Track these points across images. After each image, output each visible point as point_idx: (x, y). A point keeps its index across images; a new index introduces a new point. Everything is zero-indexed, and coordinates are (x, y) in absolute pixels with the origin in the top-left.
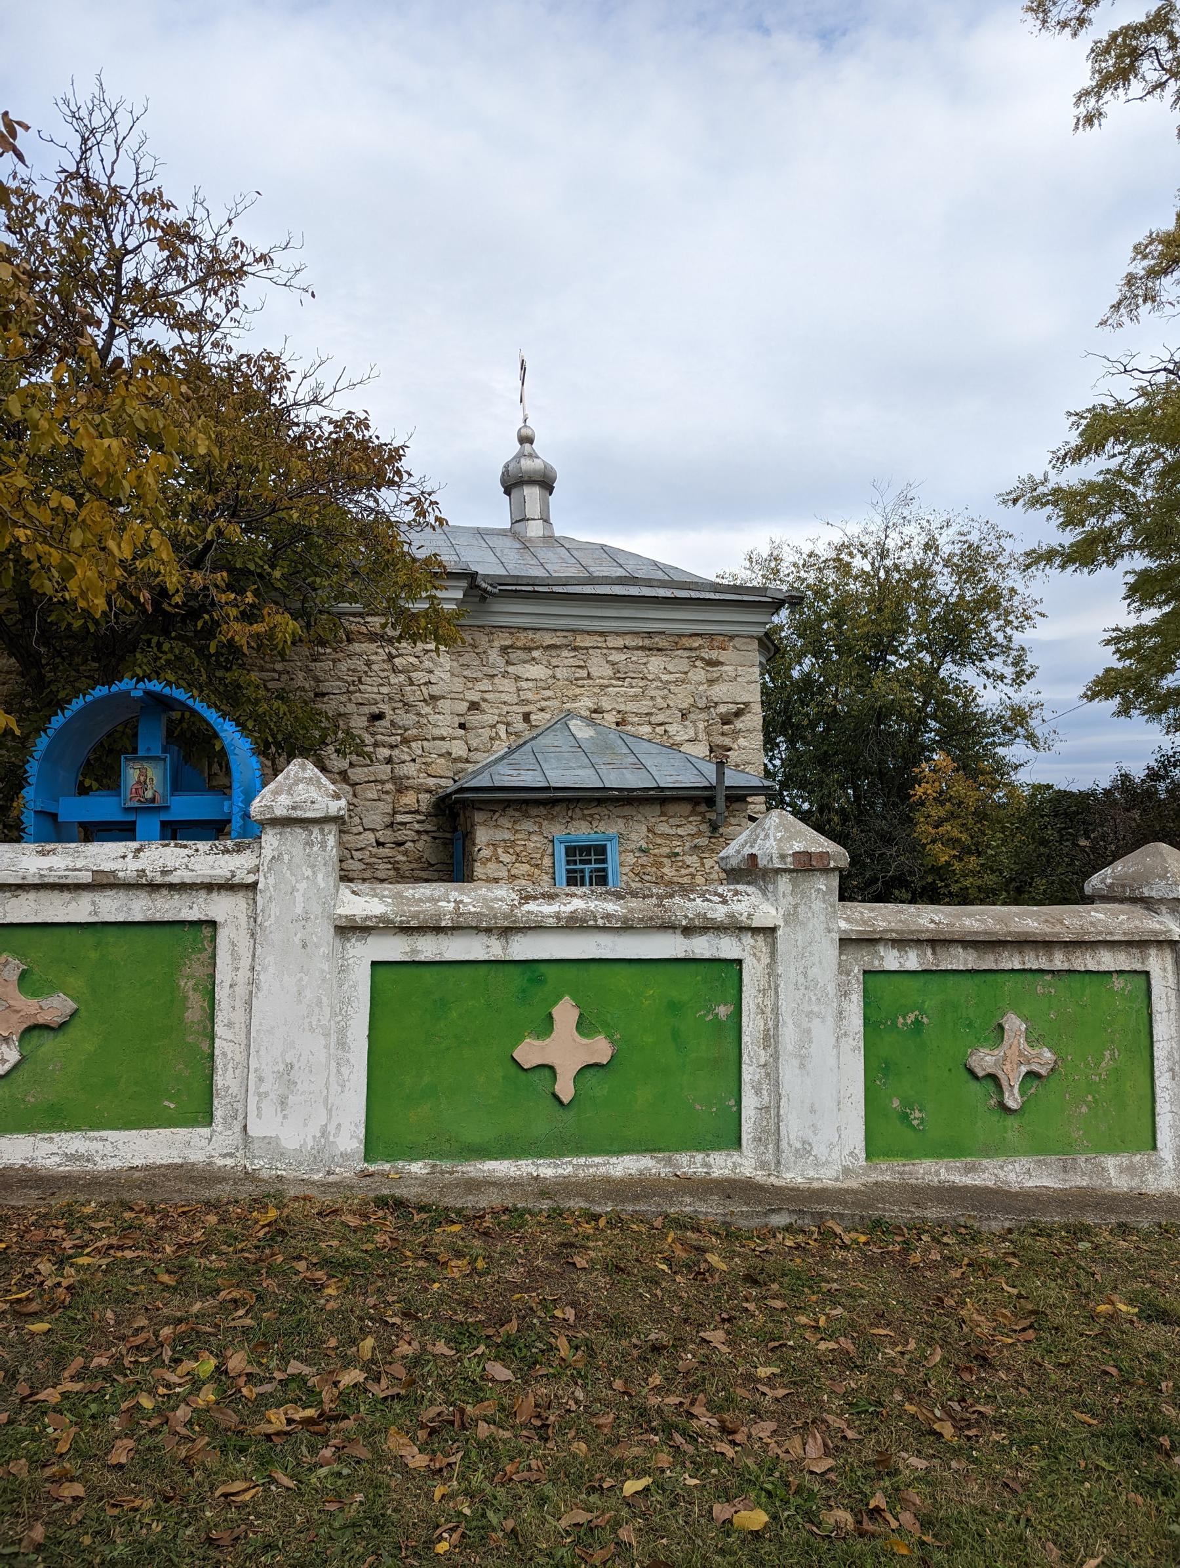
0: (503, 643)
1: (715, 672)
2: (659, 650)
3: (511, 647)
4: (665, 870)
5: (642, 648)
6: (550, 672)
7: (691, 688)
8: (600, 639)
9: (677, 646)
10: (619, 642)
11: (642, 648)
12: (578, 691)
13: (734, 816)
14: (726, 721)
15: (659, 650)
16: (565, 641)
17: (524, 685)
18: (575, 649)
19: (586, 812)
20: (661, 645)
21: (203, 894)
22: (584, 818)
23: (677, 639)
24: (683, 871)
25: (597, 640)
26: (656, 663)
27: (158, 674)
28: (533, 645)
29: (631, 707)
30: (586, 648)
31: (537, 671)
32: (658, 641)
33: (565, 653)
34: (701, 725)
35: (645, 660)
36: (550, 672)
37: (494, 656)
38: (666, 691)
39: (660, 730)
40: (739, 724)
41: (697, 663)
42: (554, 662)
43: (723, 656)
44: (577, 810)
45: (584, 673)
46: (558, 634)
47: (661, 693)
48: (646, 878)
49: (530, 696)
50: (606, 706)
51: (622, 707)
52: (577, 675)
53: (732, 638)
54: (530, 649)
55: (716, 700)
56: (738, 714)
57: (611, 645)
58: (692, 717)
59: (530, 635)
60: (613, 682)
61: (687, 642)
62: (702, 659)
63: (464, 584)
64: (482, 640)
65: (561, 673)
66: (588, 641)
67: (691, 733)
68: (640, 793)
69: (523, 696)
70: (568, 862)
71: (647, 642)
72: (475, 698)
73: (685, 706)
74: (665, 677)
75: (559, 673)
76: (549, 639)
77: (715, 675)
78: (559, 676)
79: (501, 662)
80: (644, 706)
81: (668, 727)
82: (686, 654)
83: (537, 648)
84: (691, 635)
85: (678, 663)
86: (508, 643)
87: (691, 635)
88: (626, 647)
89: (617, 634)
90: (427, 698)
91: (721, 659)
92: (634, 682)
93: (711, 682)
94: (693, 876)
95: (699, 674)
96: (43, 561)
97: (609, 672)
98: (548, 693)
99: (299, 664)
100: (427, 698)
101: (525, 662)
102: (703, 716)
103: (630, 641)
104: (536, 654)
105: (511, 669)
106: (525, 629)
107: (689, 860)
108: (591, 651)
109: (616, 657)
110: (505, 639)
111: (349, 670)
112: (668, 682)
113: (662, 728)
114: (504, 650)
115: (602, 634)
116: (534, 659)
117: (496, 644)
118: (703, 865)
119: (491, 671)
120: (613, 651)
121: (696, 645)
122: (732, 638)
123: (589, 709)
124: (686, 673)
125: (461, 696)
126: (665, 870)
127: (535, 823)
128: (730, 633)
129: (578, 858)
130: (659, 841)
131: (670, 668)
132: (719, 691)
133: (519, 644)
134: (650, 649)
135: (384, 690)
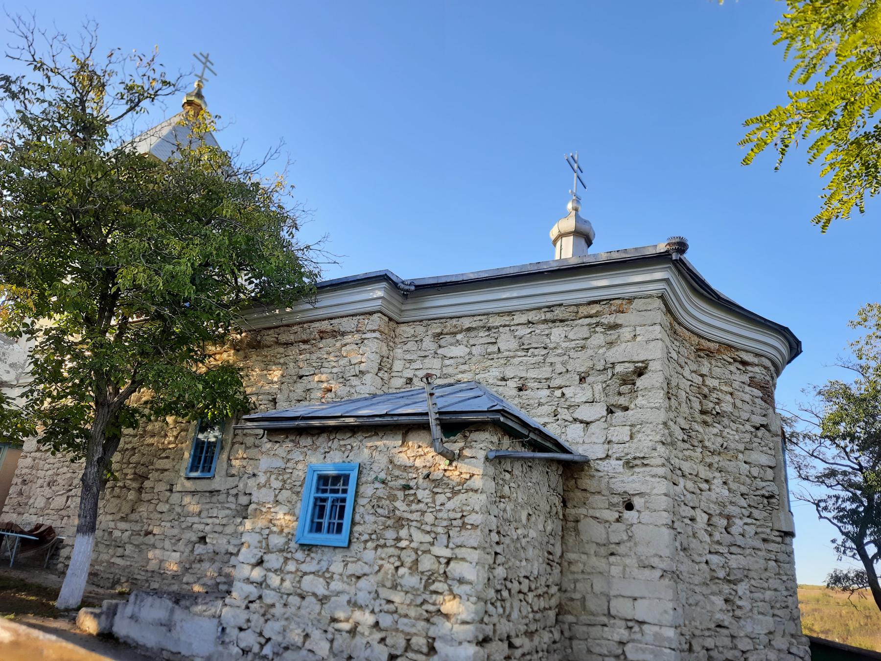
1: (613, 335)
2: (562, 321)
3: (441, 334)
4: (398, 504)
5: (545, 321)
6: (468, 350)
7: (590, 352)
9: (577, 317)
10: (523, 319)
11: (545, 321)
12: (489, 363)
13: (471, 447)
14: (625, 380)
15: (562, 321)
16: (481, 324)
17: (447, 362)
18: (489, 329)
19: (342, 443)
20: (561, 317)
21: (331, 550)
22: (292, 441)
23: (574, 309)
24: (414, 507)
25: (506, 319)
26: (557, 333)
28: (455, 330)
29: (532, 374)
30: (497, 327)
31: (460, 351)
32: (558, 313)
33: (481, 334)
34: (598, 387)
35: (547, 332)
36: (468, 350)
37: (428, 344)
38: (566, 357)
39: (558, 393)
40: (641, 382)
41: (597, 329)
42: (472, 342)
43: (620, 319)
45: (494, 348)
46: (475, 318)
47: (561, 359)
48: (380, 511)
49: (450, 370)
50: (509, 373)
51: (523, 374)
52: (489, 350)
53: (630, 300)
54: (454, 334)
55: (612, 361)
56: (640, 373)
58: (589, 379)
59: (454, 322)
60: (520, 353)
61: (583, 311)
62: (603, 325)
63: (384, 284)
66: (495, 321)
67: (588, 395)
68: (366, 420)
70: (318, 490)
71: (549, 316)
73: (583, 369)
74: (564, 345)
75: (476, 350)
76: (466, 323)
77: (614, 337)
78: (474, 352)
79: (433, 346)
80: (545, 372)
81: (564, 390)
83: (461, 332)
85: (579, 331)
86: (438, 331)
88: (529, 322)
89: (522, 311)
91: (619, 322)
92: (536, 352)
93: (611, 344)
94: (423, 513)
95: (599, 339)
96: (608, 388)
97: (514, 344)
98: (466, 367)
102: (602, 378)
103: (533, 316)
104: (459, 337)
105: (440, 351)
106: (451, 318)
107: (421, 494)
108: (501, 329)
109: (523, 331)
111: (318, 358)
113: (560, 391)
115: (510, 313)
117: (429, 333)
118: (434, 502)
119: (423, 354)
120: (519, 327)
121: (594, 311)
122: (630, 300)
123: (496, 377)
125: (400, 374)
126: (398, 504)
128: (627, 296)
129: (329, 487)
131: (571, 336)
132: (614, 354)
133: (445, 331)
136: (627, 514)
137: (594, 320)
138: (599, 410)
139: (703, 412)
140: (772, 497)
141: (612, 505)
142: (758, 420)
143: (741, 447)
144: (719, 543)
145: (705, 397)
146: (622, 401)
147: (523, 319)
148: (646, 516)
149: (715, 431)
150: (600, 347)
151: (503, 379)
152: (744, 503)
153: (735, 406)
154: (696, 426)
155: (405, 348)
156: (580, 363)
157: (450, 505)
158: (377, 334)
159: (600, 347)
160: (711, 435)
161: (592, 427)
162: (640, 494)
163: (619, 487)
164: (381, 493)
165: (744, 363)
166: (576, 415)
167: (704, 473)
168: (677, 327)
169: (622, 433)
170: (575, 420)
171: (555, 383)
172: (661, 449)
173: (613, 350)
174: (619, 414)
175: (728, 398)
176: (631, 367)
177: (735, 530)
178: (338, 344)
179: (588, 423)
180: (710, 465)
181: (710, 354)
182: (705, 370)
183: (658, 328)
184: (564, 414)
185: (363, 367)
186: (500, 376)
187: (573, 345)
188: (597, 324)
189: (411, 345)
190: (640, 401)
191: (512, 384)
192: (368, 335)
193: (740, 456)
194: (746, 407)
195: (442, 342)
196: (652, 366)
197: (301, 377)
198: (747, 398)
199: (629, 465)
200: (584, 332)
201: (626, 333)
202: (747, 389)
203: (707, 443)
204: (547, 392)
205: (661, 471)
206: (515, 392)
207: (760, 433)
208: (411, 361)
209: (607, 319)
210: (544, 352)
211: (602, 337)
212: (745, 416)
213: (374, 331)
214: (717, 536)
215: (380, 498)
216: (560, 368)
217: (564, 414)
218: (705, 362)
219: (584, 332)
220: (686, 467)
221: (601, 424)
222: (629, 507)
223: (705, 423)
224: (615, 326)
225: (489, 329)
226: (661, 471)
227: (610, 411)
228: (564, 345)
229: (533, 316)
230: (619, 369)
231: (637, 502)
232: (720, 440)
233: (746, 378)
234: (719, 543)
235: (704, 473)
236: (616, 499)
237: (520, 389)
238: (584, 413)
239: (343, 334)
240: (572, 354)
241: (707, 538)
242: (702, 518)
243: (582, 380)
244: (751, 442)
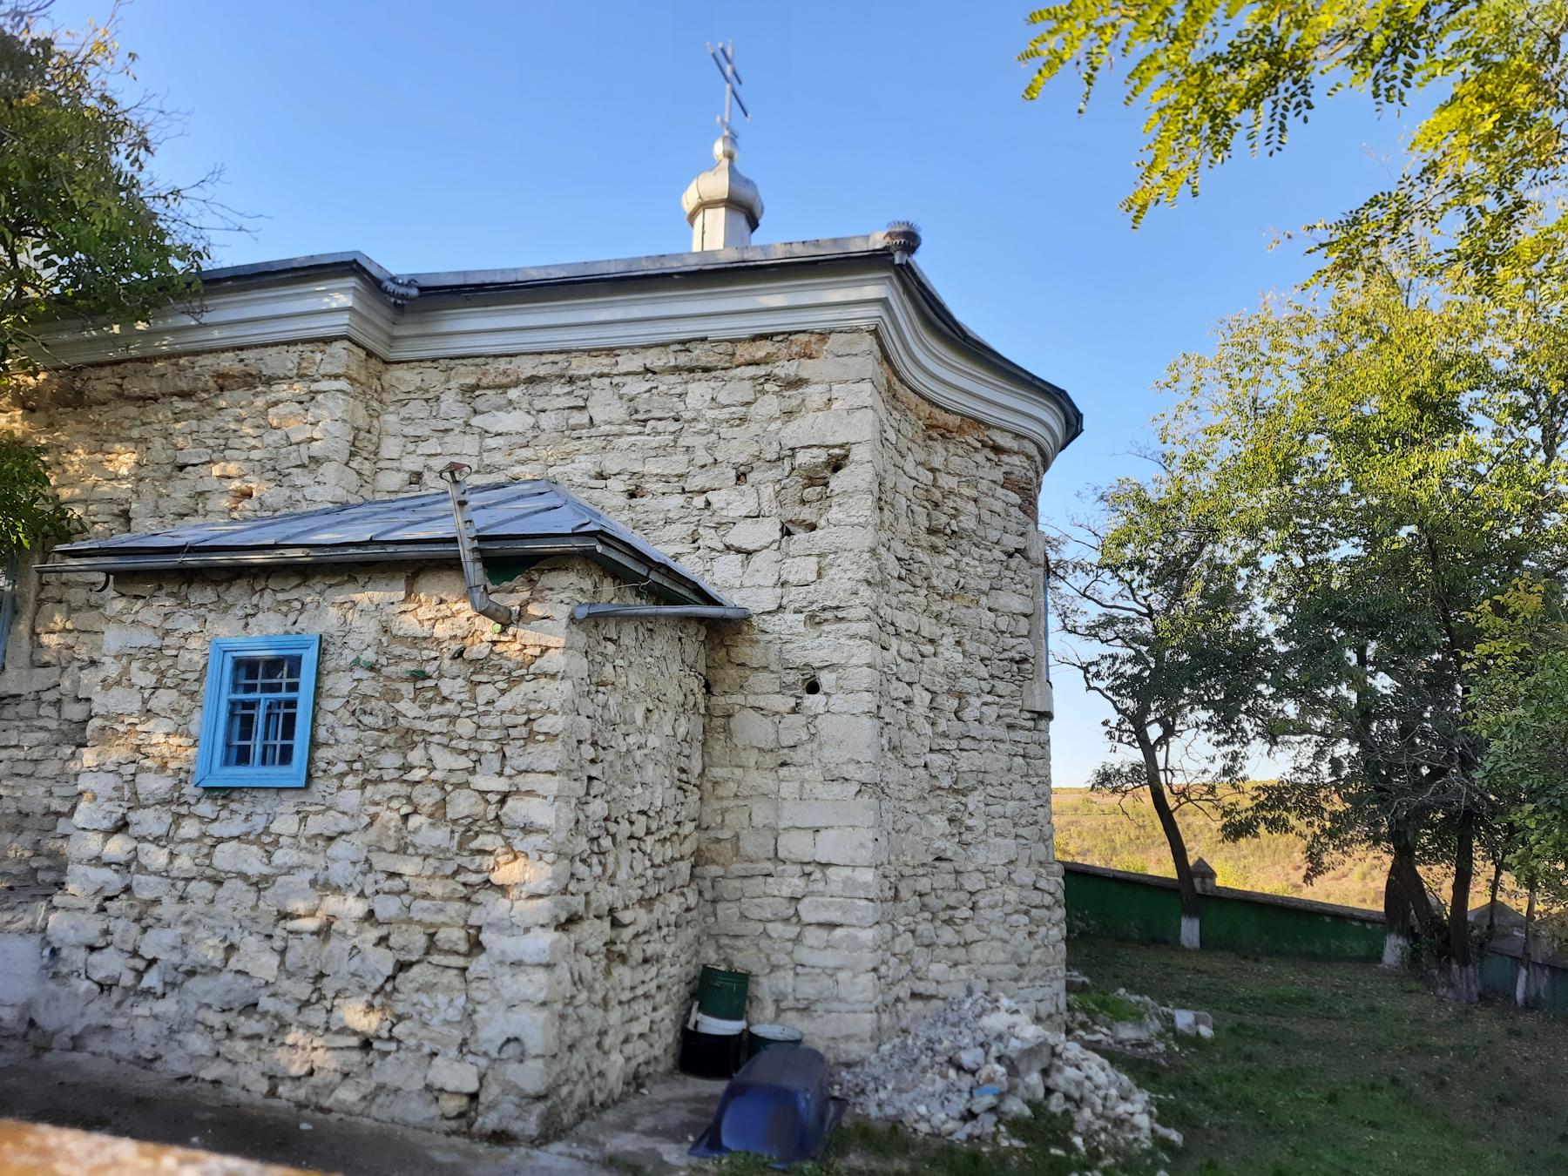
0: (462, 381)
1: (793, 398)
2: (706, 370)
3: (478, 387)
4: (402, 706)
5: (676, 369)
6: (531, 421)
7: (754, 428)
8: (606, 361)
10: (634, 363)
11: (676, 369)
15: (706, 370)
16: (555, 370)
17: (491, 442)
18: (571, 381)
19: (281, 597)
20: (704, 361)
23: (729, 348)
24: (435, 709)
26: (699, 391)
27: (1317, 680)
28: (505, 380)
29: (652, 467)
30: (587, 378)
32: (700, 355)
33: (558, 389)
34: (768, 491)
35: (679, 390)
36: (531, 421)
37: (451, 404)
39: (699, 501)
40: (837, 482)
41: (767, 387)
42: (539, 404)
43: (806, 369)
44: (267, 593)
45: (580, 418)
46: (544, 359)
47: (704, 440)
48: (367, 720)
49: (498, 458)
50: (611, 466)
51: (638, 468)
52: (571, 422)
53: (824, 335)
54: (504, 388)
56: (836, 465)
57: (622, 368)
58: (752, 477)
59: (502, 364)
61: (745, 352)
63: (352, 282)
64: (434, 377)
65: (547, 421)
67: (750, 505)
69: (488, 459)
71: (683, 359)
72: (416, 468)
73: (742, 459)
74: (710, 414)
75: (547, 421)
76: (527, 367)
77: (795, 402)
78: (543, 424)
79: (461, 411)
80: (677, 463)
81: (710, 496)
82: (752, 370)
83: (516, 384)
84: (756, 338)
85: (736, 389)
86: (472, 380)
87: (756, 338)
88: (647, 370)
89: (632, 349)
90: (306, 461)
91: (804, 375)
92: (660, 426)
95: (770, 404)
97: (619, 411)
99: (157, 427)
100: (306, 461)
101: (499, 408)
103: (654, 359)
104: (513, 394)
105: (475, 421)
106: (496, 356)
107: (446, 687)
108: (594, 382)
109: (635, 386)
110: (467, 375)
112: (716, 422)
113: (702, 498)
114: (470, 391)
115: (610, 351)
116: (510, 402)
117: (453, 384)
118: (474, 699)
119: (442, 425)
120: (628, 379)
121: (761, 354)
122: (824, 335)
124: (748, 404)
125: (396, 464)
126: (402, 706)
127: (195, 618)
128: (818, 327)
129: (259, 681)
130: (398, 650)
131: (723, 398)
132: (794, 433)
133: (484, 382)
134: (691, 370)
135: (255, 455)
136: (810, 700)
137: (761, 371)
138: (769, 530)
139: (931, 531)
140: (1024, 660)
141: (785, 687)
142: (1012, 542)
143: (985, 585)
144: (945, 735)
145: (936, 505)
146: (807, 514)
147: (634, 363)
148: (838, 702)
149: (948, 561)
150: (772, 419)
151: (601, 476)
152: (983, 672)
153: (980, 520)
154: (921, 555)
155: (404, 412)
156: (737, 448)
157: (505, 703)
158: (342, 384)
159: (772, 419)
160: (941, 570)
161: (756, 558)
162: (831, 667)
163: (797, 657)
164: (367, 687)
165: (998, 449)
166: (729, 540)
167: (929, 628)
168: (897, 386)
169: (804, 569)
170: (728, 548)
171: (693, 484)
172: (865, 592)
173: (793, 425)
174: (801, 536)
175: (971, 507)
176: (822, 456)
177: (968, 714)
178: (260, 402)
179: (749, 553)
180: (938, 616)
181: (946, 434)
182: (937, 462)
183: (867, 387)
184: (709, 538)
185: (316, 448)
186: (594, 470)
187: (724, 414)
188: (768, 378)
189: (416, 408)
190: (835, 514)
191: (616, 485)
192: (324, 385)
193: (983, 599)
194: (997, 522)
195: (480, 404)
196: (858, 454)
197: (182, 468)
198: (998, 506)
199: (814, 620)
200: (745, 392)
201: (814, 394)
202: (1000, 492)
203: (935, 581)
204: (680, 500)
205: (863, 628)
206: (622, 500)
207: (1013, 563)
208: (417, 439)
209: (785, 369)
210: (675, 426)
211: (775, 400)
212: (994, 535)
213: (337, 377)
214: (943, 726)
215: (366, 698)
216: (702, 457)
217: (709, 538)
218: (938, 446)
219: (745, 392)
220: (902, 620)
221: (770, 555)
222: (813, 688)
223: (934, 548)
224: (797, 383)
225: (571, 381)
226: (863, 628)
227: (787, 533)
228: (710, 414)
229: (654, 359)
230: (802, 458)
231: (826, 679)
232: (954, 575)
233: (998, 475)
234: (945, 735)
235: (929, 628)
236: (791, 678)
237: (632, 495)
238: (743, 536)
239: (269, 381)
240: (725, 431)
241: (928, 730)
242: (922, 699)
243: (741, 477)
244: (1000, 577)
